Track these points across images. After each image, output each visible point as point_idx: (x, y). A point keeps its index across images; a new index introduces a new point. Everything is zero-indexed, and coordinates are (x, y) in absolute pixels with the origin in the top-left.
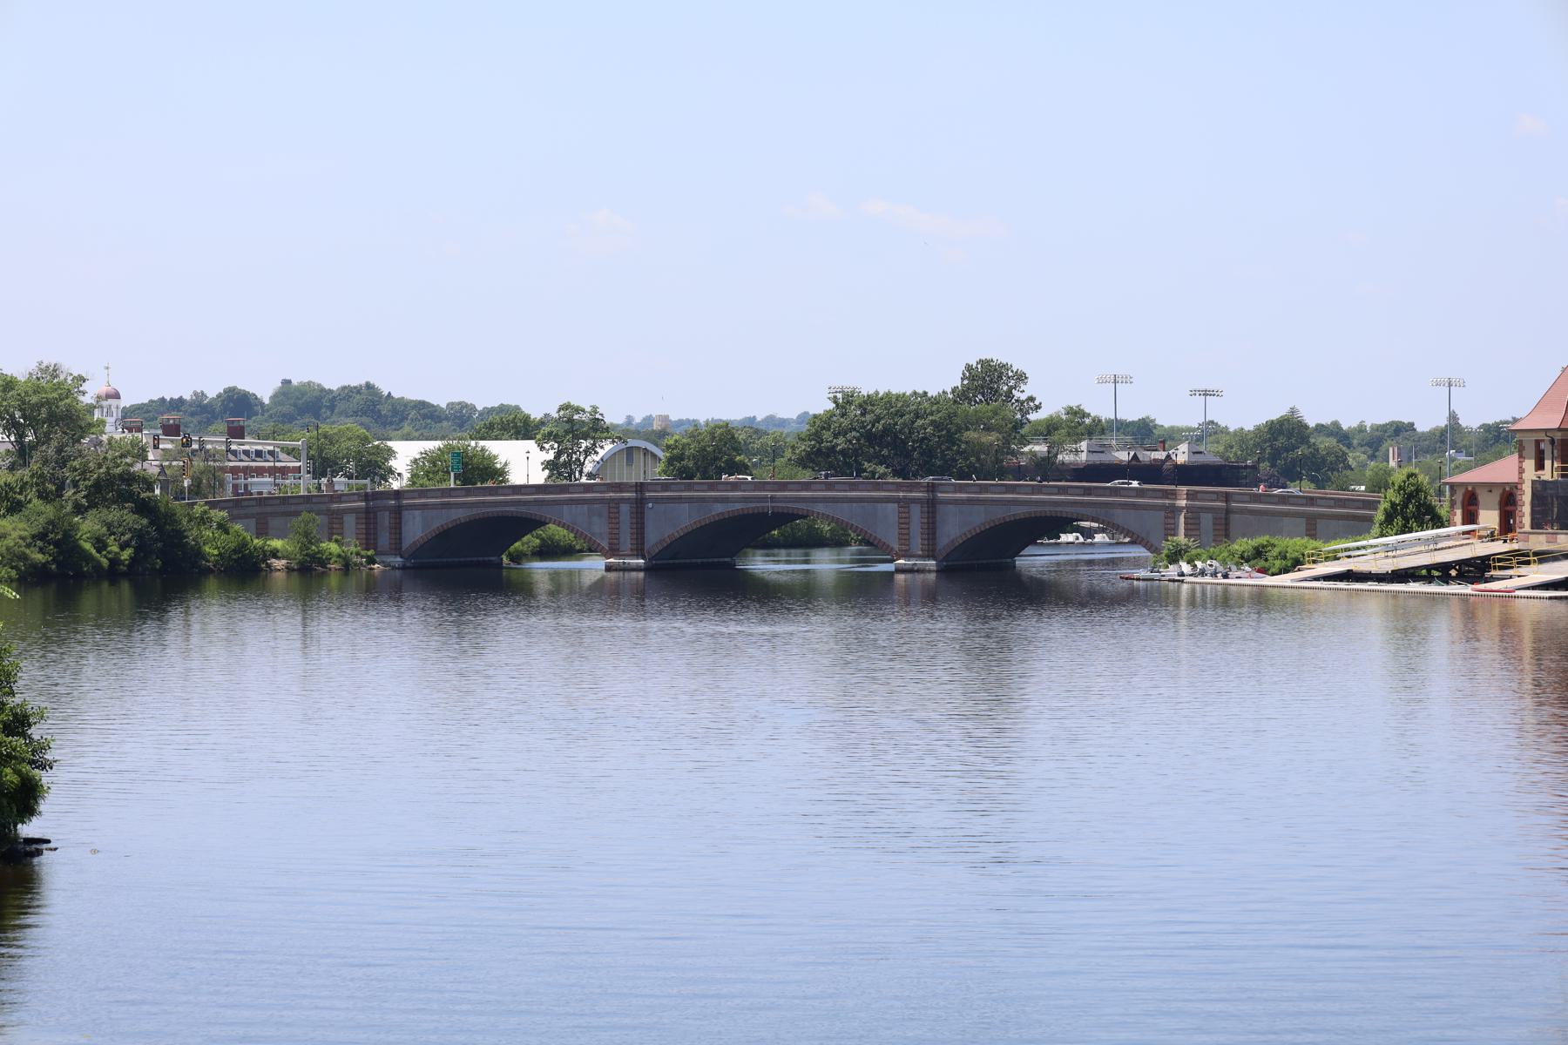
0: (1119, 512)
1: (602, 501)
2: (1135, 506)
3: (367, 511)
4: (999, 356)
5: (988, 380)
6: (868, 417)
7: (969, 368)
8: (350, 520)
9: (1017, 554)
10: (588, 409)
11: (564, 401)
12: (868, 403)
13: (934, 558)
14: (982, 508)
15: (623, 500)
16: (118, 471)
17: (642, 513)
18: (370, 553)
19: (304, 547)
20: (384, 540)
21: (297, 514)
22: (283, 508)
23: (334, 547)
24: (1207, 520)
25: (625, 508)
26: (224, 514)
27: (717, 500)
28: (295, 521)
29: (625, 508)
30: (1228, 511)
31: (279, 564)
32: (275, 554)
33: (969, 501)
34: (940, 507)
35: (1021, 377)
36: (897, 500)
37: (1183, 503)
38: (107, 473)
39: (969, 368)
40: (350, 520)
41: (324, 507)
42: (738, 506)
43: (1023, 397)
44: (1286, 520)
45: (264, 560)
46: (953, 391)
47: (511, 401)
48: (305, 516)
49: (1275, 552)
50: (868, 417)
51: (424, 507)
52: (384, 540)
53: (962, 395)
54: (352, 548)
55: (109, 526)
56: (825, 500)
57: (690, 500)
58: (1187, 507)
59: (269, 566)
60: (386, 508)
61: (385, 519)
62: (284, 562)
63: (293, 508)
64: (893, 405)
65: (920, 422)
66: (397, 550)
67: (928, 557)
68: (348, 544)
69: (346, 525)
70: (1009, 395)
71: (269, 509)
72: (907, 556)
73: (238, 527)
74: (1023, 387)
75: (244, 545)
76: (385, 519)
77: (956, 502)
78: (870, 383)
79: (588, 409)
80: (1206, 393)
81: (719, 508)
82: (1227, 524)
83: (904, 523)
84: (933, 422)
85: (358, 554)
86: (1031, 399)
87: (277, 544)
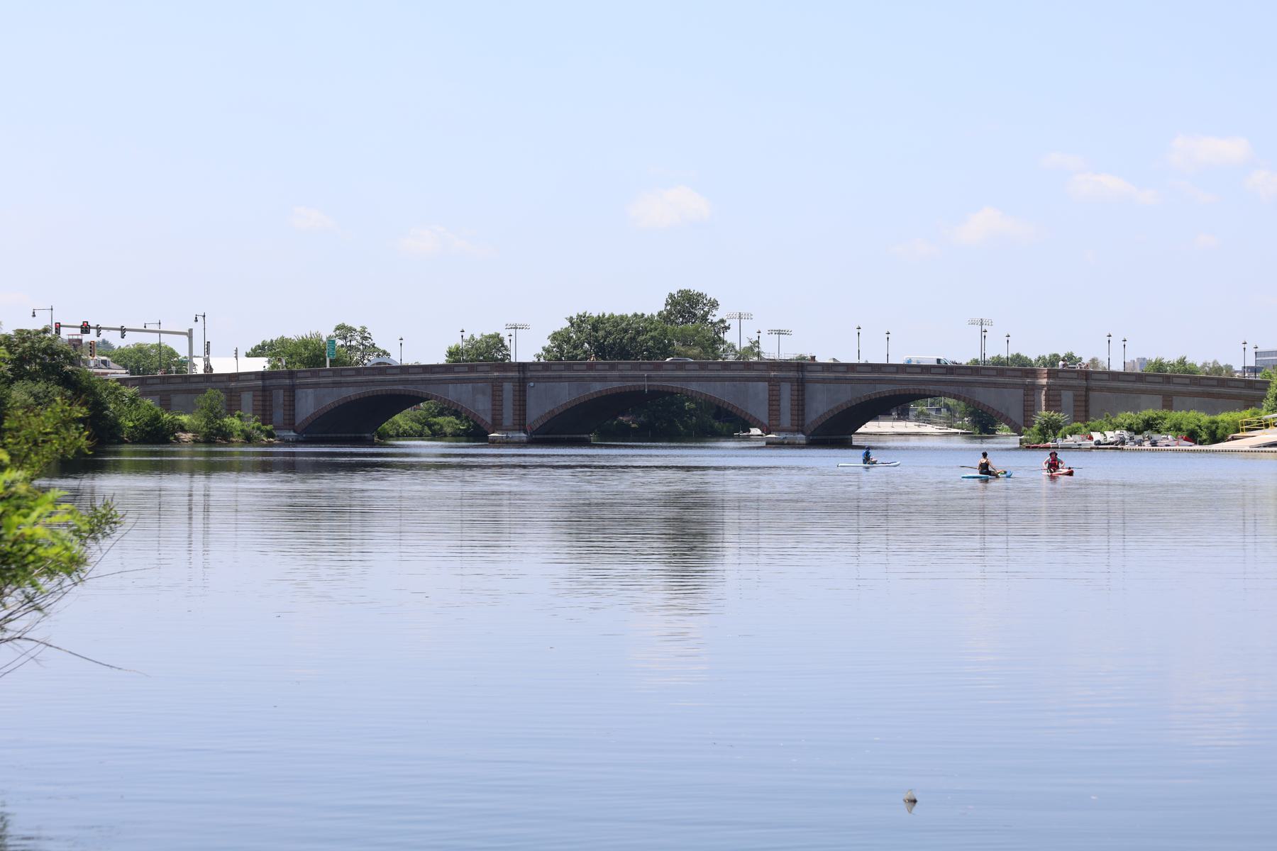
0: (979, 390)
1: (485, 380)
2: (995, 385)
3: (264, 389)
4: (696, 288)
5: (687, 306)
6: (601, 333)
7: (671, 296)
8: (247, 398)
9: (853, 432)
10: (359, 329)
11: (339, 323)
12: (597, 323)
13: (803, 433)
14: (849, 386)
15: (505, 379)
16: (43, 345)
17: (525, 391)
18: (269, 427)
19: (210, 421)
20: (279, 415)
21: (204, 391)
22: (185, 386)
23: (236, 422)
24: (1067, 397)
25: (508, 387)
26: (136, 389)
27: (595, 379)
28: (201, 398)
29: (508, 387)
30: (1088, 389)
31: (187, 437)
32: (182, 428)
33: (837, 380)
34: (809, 387)
35: (714, 304)
36: (769, 380)
37: (1044, 381)
38: (32, 347)
39: (671, 296)
40: (247, 398)
41: (222, 385)
42: (616, 384)
43: (716, 320)
44: (1143, 396)
45: (173, 434)
46: (659, 314)
47: (310, 322)
48: (210, 391)
49: (1167, 424)
50: (601, 333)
51: (316, 385)
52: (279, 415)
53: (666, 318)
54: (252, 424)
55: (36, 396)
56: (698, 379)
57: (569, 379)
58: (1048, 385)
59: (177, 439)
60: (279, 387)
61: (280, 397)
62: (190, 435)
63: (194, 386)
64: (618, 324)
65: (641, 338)
66: (290, 425)
67: (798, 431)
68: (249, 419)
69: (243, 403)
70: (704, 318)
71: (172, 387)
72: (779, 430)
73: (149, 401)
74: (715, 312)
75: (157, 418)
76: (280, 397)
77: (823, 381)
78: (596, 309)
79: (359, 329)
80: (779, 332)
81: (597, 387)
82: (1087, 401)
83: (774, 401)
84: (652, 338)
85: (258, 428)
86: (722, 321)
87: (185, 419)
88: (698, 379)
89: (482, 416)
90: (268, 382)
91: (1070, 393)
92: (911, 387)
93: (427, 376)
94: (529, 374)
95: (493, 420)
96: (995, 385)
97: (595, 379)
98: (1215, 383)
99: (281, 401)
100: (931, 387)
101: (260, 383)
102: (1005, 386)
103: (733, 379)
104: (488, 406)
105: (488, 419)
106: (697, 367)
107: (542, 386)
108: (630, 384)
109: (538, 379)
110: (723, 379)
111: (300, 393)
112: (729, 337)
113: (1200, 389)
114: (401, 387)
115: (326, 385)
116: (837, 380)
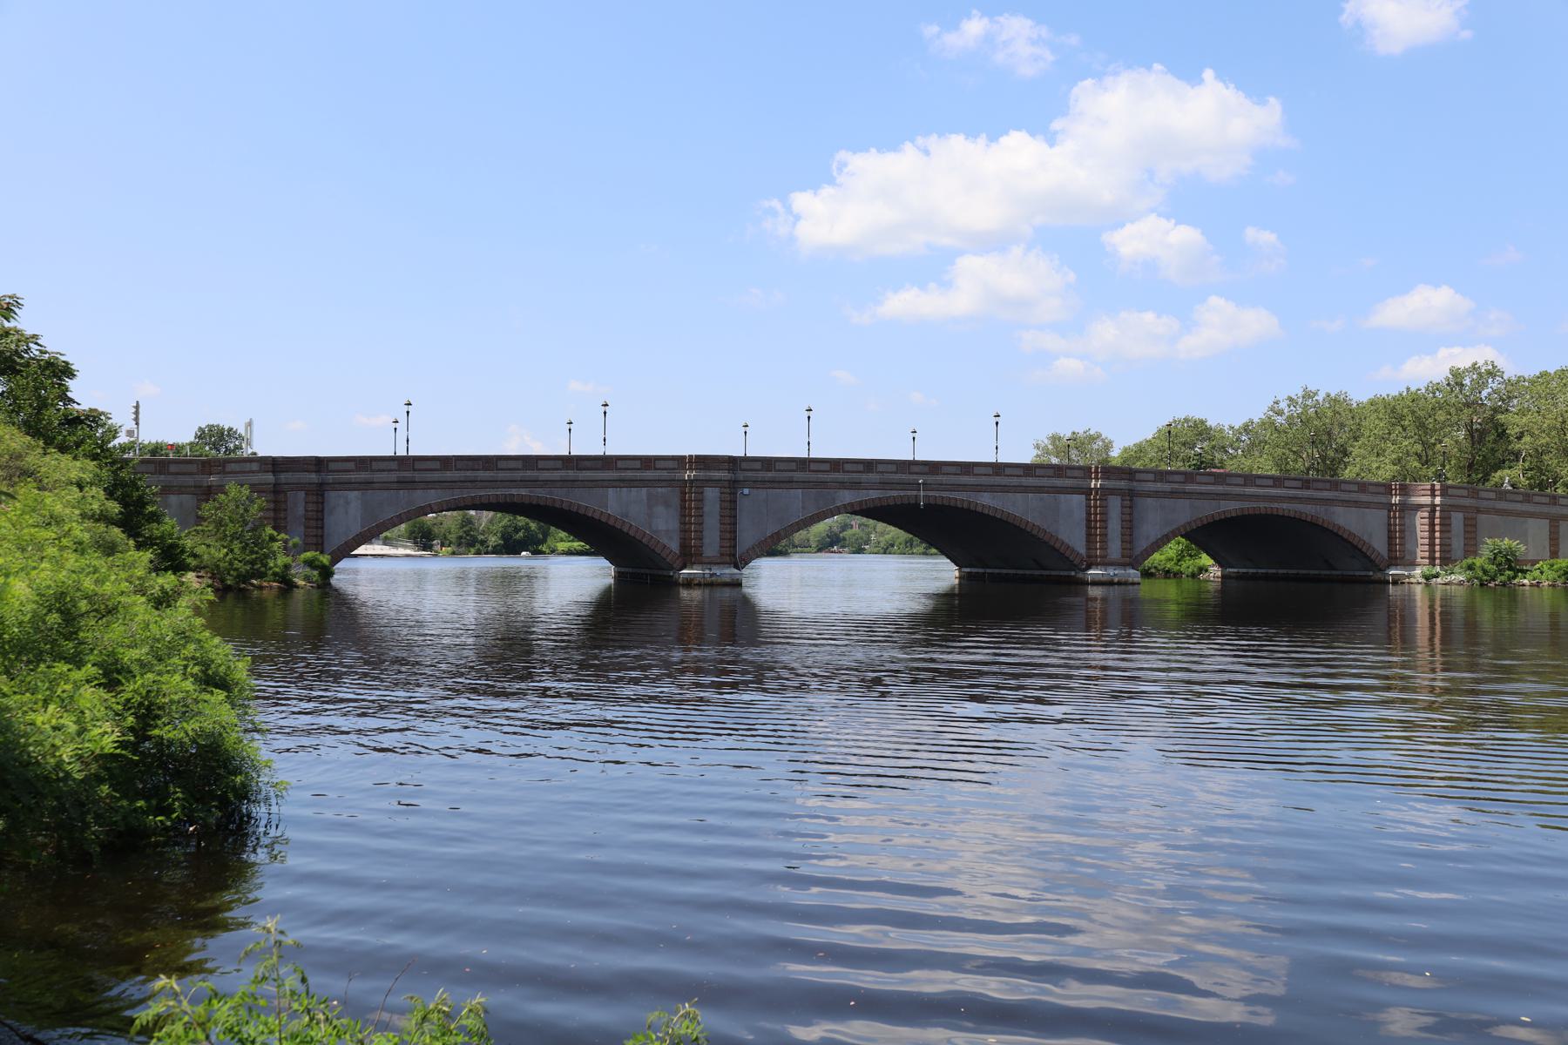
0: (1339, 510)
1: (670, 483)
3: (277, 491)
15: (709, 482)
22: (363, 476)
25: (711, 494)
29: (711, 494)
44: (1531, 521)
60: (299, 486)
63: (501, 475)
77: (1157, 494)
88: (992, 489)
89: (664, 541)
90: (283, 477)
91: (1460, 515)
92: (1262, 505)
93: (571, 474)
94: (330, 478)
95: (684, 546)
96: (1357, 504)
97: (843, 485)
98: (894, 468)
99: (301, 510)
100: (1285, 506)
101: (270, 478)
102: (1368, 505)
103: (1039, 490)
104: (674, 524)
105: (674, 546)
106: (1270, 482)
107: (762, 494)
108: (895, 493)
109: (756, 484)
110: (1025, 489)
111: (332, 497)
112: (108, 744)
113: (1167, 487)
114: (523, 492)
115: (385, 486)
116: (1173, 494)
